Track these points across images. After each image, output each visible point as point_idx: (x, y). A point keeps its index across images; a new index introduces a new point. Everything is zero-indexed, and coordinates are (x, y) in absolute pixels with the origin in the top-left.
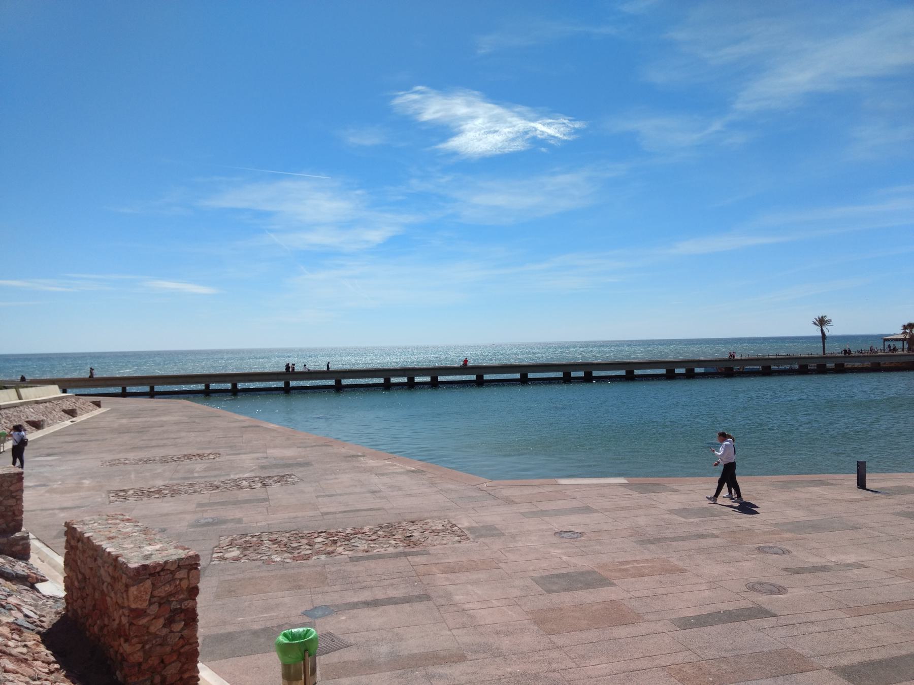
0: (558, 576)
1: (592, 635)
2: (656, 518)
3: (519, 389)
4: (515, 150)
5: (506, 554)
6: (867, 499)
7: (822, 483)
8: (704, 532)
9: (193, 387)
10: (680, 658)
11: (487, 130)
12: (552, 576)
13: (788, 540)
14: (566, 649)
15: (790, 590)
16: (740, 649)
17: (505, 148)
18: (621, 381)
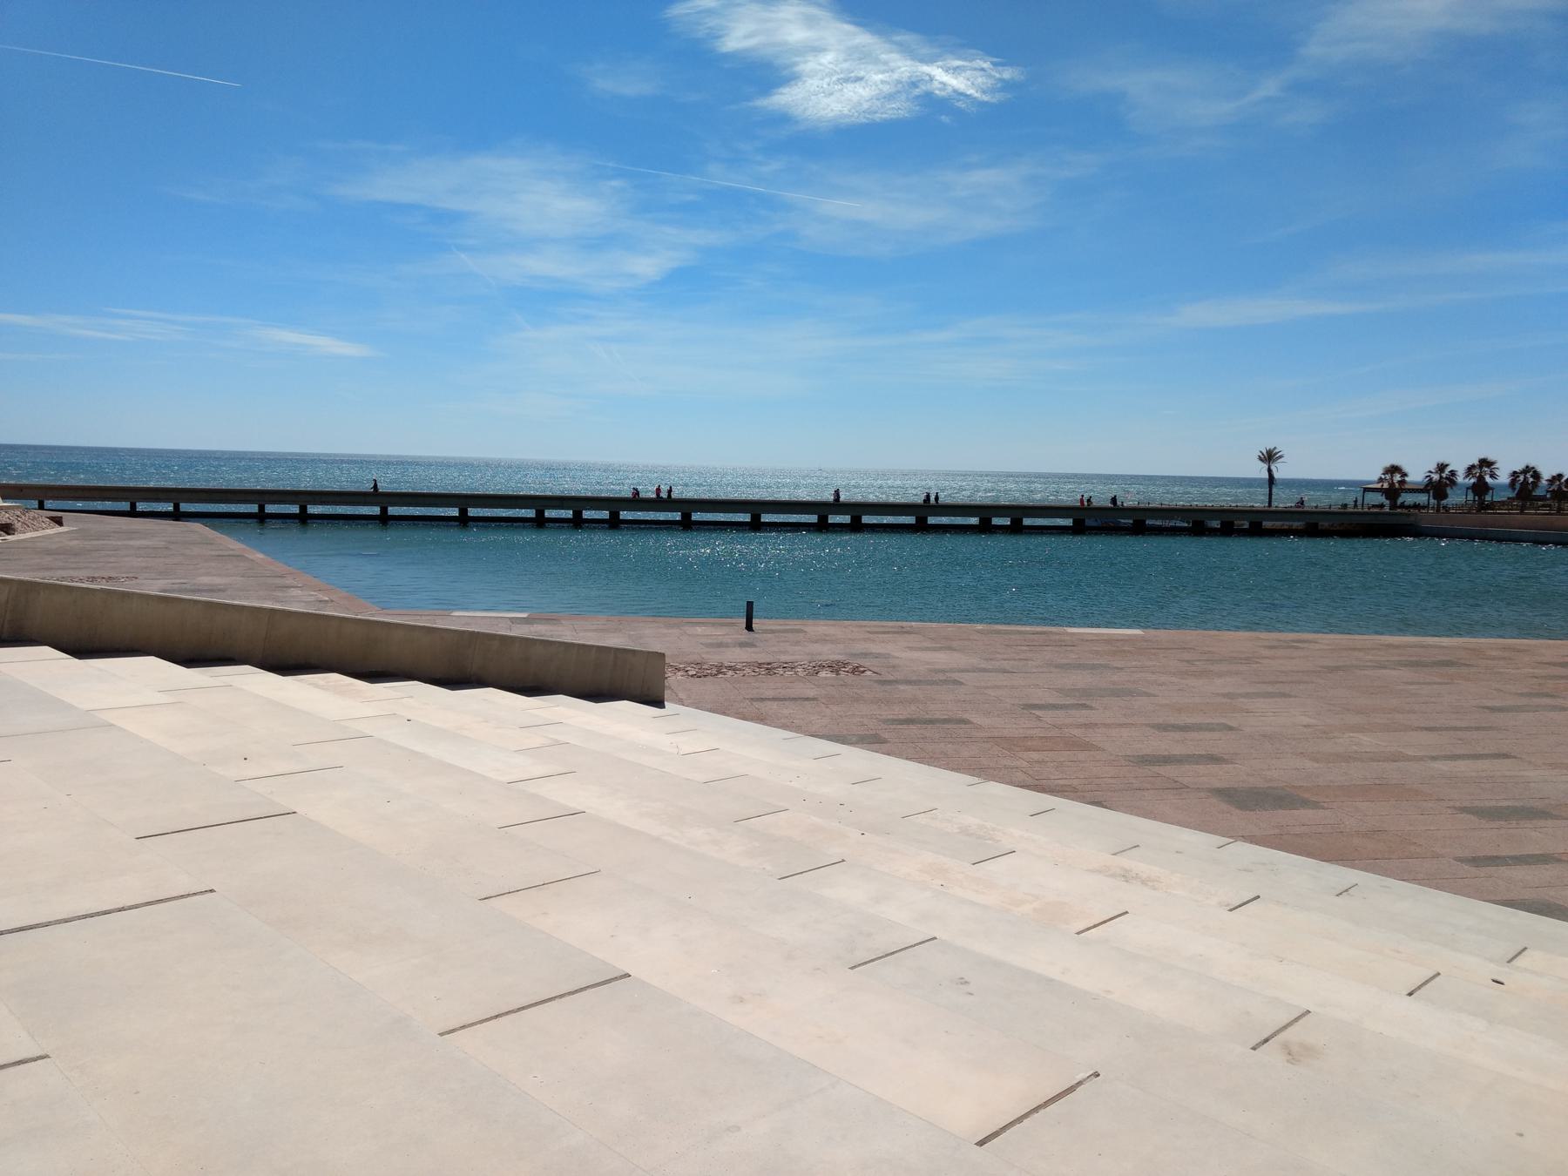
3: (528, 537)
4: (893, 116)
9: (944, 520)
11: (842, 76)
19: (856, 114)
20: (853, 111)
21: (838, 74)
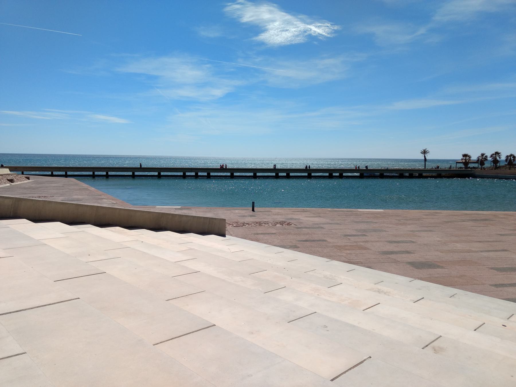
4: (298, 42)
11: (281, 29)
17: (293, 41)
18: (357, 178)
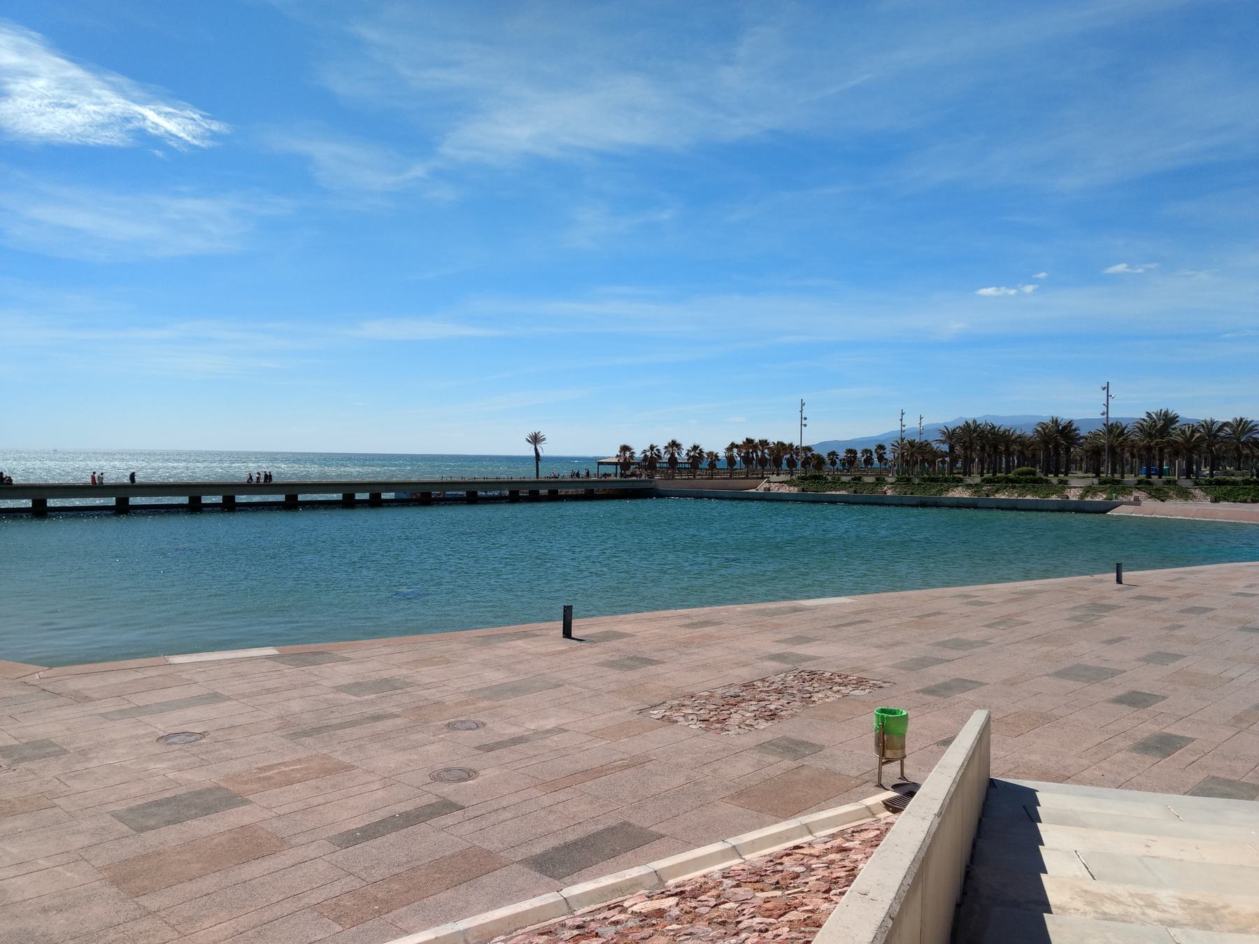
0: (158, 804)
1: (209, 883)
2: (315, 700)
4: (107, 143)
5: (67, 782)
6: (572, 650)
7: (526, 635)
8: (381, 712)
10: (337, 888)
12: (149, 805)
13: (485, 709)
14: (163, 914)
15: (481, 773)
16: (418, 860)
19: (69, 135)
20: (65, 132)
21: (50, 98)
